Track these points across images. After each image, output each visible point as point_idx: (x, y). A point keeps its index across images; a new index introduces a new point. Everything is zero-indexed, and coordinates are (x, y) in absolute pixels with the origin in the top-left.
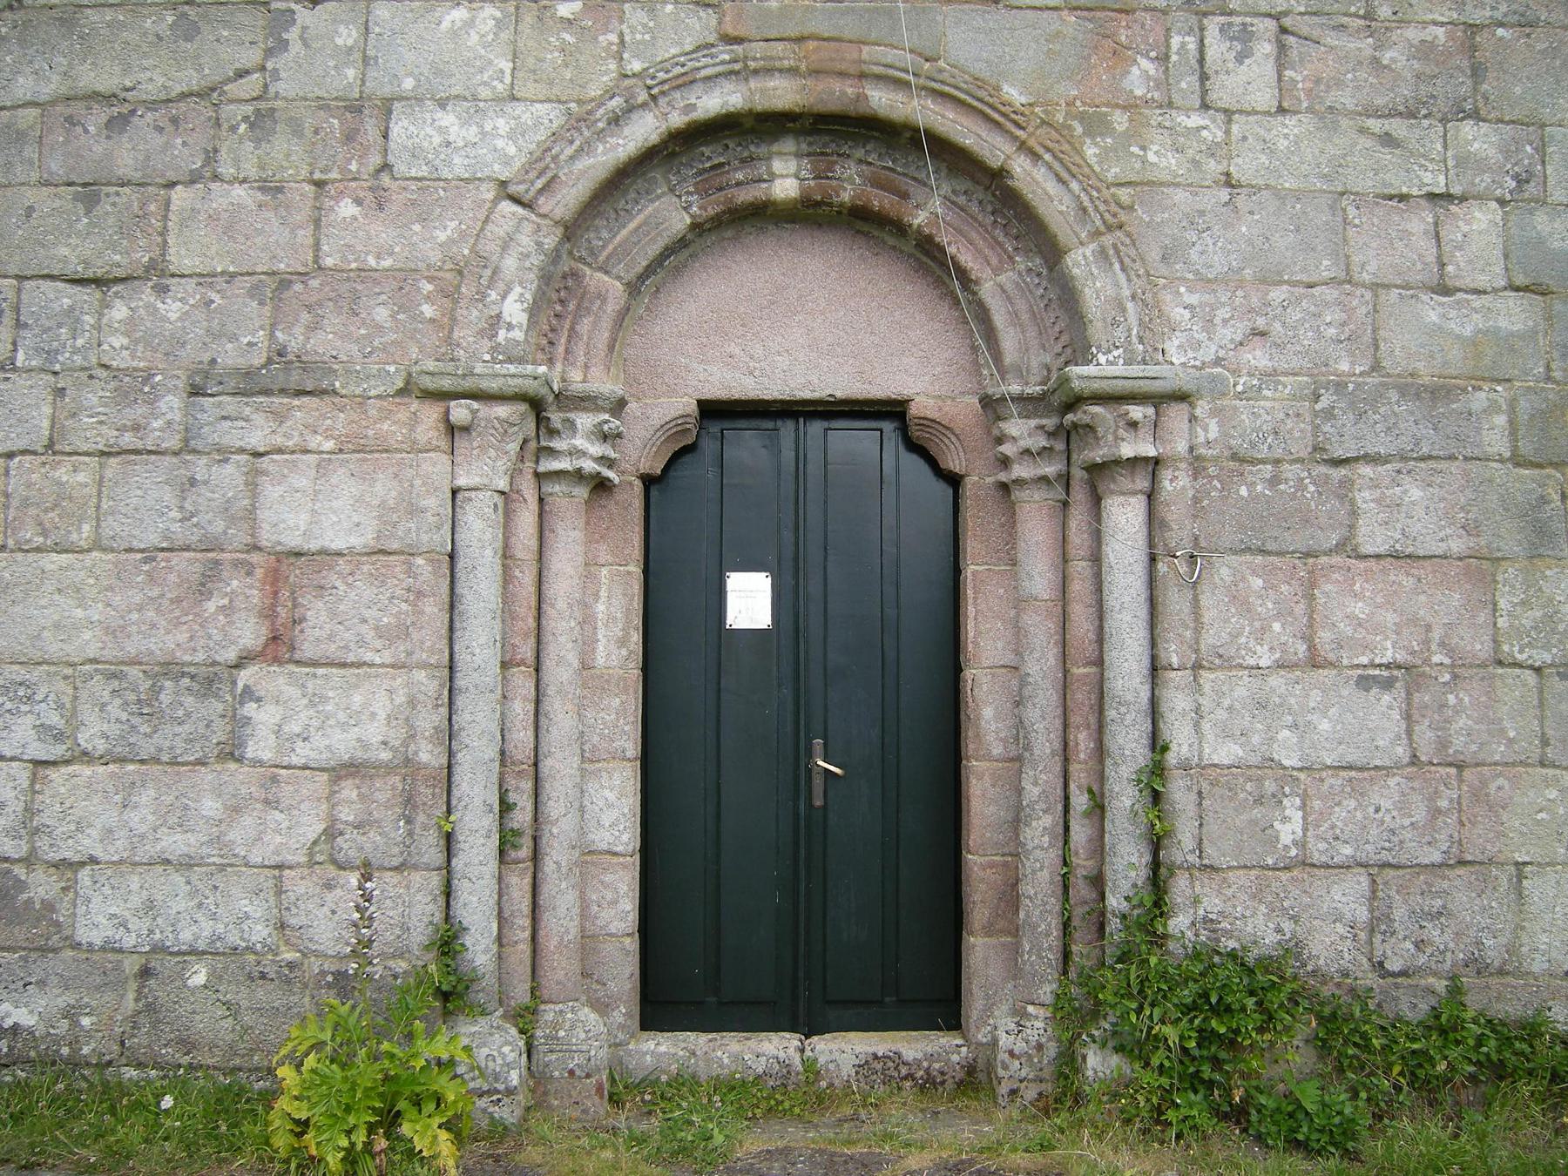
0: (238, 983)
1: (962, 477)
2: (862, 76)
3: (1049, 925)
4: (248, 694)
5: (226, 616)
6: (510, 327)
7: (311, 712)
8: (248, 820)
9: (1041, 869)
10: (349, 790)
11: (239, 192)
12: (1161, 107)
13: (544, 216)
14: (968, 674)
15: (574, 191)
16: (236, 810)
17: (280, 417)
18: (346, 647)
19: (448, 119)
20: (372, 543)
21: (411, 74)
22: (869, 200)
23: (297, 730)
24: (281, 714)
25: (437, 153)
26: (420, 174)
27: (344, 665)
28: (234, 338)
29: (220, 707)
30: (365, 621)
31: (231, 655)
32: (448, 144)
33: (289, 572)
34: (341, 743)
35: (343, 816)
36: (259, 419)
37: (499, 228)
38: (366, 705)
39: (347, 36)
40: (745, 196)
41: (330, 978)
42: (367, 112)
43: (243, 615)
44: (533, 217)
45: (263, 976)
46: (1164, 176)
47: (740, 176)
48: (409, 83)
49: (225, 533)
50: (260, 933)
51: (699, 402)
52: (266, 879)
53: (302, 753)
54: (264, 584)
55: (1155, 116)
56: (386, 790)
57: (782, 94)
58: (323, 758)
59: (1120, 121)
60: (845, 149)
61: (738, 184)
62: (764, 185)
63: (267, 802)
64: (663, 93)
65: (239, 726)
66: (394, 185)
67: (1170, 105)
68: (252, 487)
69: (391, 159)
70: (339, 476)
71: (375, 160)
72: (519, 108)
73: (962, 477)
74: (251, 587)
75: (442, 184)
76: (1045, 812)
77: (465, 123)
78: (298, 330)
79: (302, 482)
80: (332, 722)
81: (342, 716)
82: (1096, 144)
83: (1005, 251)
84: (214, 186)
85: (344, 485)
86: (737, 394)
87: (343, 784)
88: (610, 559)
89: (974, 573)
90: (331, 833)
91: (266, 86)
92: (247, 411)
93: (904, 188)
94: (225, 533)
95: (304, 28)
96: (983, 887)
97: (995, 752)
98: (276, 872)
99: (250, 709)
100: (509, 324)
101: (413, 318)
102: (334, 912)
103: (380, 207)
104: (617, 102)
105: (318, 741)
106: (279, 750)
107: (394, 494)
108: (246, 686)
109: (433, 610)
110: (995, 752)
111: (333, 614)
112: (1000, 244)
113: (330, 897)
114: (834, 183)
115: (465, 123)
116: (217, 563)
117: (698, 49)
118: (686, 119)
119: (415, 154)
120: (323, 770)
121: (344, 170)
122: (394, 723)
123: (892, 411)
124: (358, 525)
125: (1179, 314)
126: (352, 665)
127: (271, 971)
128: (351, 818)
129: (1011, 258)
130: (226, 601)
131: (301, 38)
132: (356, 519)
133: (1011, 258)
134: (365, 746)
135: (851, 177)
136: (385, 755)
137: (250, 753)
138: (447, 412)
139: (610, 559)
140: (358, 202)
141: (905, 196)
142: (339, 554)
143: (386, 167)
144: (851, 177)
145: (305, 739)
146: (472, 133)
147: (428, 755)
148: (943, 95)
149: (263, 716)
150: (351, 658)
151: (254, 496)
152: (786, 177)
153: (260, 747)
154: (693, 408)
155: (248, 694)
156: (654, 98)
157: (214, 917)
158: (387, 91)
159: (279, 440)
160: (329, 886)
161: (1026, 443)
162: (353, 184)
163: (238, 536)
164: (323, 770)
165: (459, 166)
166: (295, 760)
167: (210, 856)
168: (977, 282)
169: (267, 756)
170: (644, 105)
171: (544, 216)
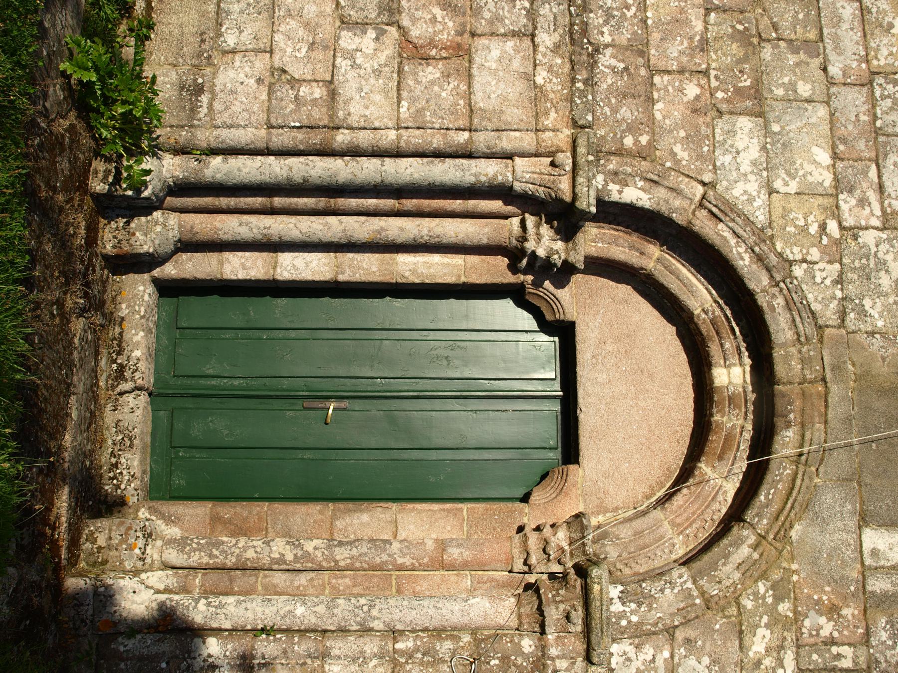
0: (199, 26)
1: (527, 502)
2: (803, 426)
3: (218, 557)
4: (381, 33)
5: (430, 19)
6: (620, 192)
7: (369, 70)
8: (301, 32)
9: (256, 552)
10: (318, 92)
11: (699, 26)
12: (797, 640)
13: (693, 213)
14: (394, 506)
15: (711, 232)
16: (307, 25)
17: (556, 48)
18: (411, 91)
19: (754, 152)
20: (477, 106)
21: (782, 128)
22: (716, 433)
23: (358, 62)
24: (369, 50)
25: (732, 146)
26: (717, 136)
27: (399, 89)
28: (606, 22)
29: (373, 16)
30: (427, 102)
31: (405, 22)
32: (738, 153)
33: (460, 54)
34: (349, 86)
35: (302, 89)
36: (556, 37)
37: (685, 184)
38: (373, 102)
39: (804, 89)
40: (714, 349)
41: (200, 81)
42: (756, 102)
43: (430, 30)
44: (693, 207)
45: (203, 41)
46: (747, 640)
47: (727, 345)
48: (776, 128)
49: (483, 18)
50: (231, 40)
51: (573, 324)
52: (264, 43)
53: (343, 64)
54: (451, 41)
55: (790, 636)
56: (319, 115)
57: (788, 363)
58: (339, 78)
59: (785, 608)
60: (751, 416)
61: (722, 345)
62: (722, 362)
63: (314, 43)
64: (781, 290)
65: (361, 26)
66: (708, 119)
67: (798, 647)
68: (514, 34)
69: (726, 117)
70: (521, 86)
71: (724, 107)
72: (764, 196)
73: (527, 502)
74: (449, 34)
75: (711, 149)
76: (295, 555)
77: (754, 163)
78: (613, 62)
79: (516, 64)
80: (363, 83)
81: (366, 89)
82: (767, 591)
83: (686, 528)
84: (702, 11)
85: (515, 89)
86: (579, 346)
87: (323, 89)
88: (469, 265)
89: (461, 510)
90: (294, 83)
91: (768, 41)
92: (561, 31)
93: (726, 457)
94: (483, 18)
95: (808, 64)
96: (245, 514)
97: (338, 523)
98: (268, 49)
99: (371, 34)
100: (622, 192)
101: (623, 131)
102: (242, 83)
103: (695, 111)
104: (773, 260)
105: (352, 74)
106: (346, 51)
107: (509, 119)
108: (386, 31)
109: (437, 141)
110: (338, 523)
111: (433, 83)
112: (690, 525)
113: (252, 81)
114: (727, 409)
115: (754, 163)
116: (464, 14)
117: (813, 313)
118: (765, 305)
119: (731, 132)
120: (333, 76)
121: (717, 89)
122: (362, 120)
123: (570, 452)
124: (489, 97)
125: (648, 652)
126: (399, 95)
127: (206, 46)
128: (301, 94)
129: (681, 532)
130: (440, 19)
131: (801, 61)
132: (493, 96)
133: (681, 532)
134: (347, 102)
135: (731, 420)
136: (341, 114)
137: (344, 33)
138: (562, 151)
139: (469, 265)
140: (697, 98)
141: (720, 458)
142: (469, 87)
143: (720, 113)
144: (731, 420)
145: (352, 66)
146: (746, 167)
147: (342, 138)
148: (794, 480)
149: (368, 40)
150: (404, 94)
151: (504, 35)
152: (732, 374)
153: (348, 40)
154: (569, 317)
155: (381, 33)
156: (777, 285)
157: (242, 12)
158: (771, 116)
159: (541, 49)
160: (259, 81)
161: (553, 542)
162: (708, 95)
163: (482, 26)
164: (333, 76)
165: (724, 159)
166: (339, 61)
167: (279, 10)
168: (663, 509)
169: (343, 43)
170: (772, 277)
171: (693, 213)
